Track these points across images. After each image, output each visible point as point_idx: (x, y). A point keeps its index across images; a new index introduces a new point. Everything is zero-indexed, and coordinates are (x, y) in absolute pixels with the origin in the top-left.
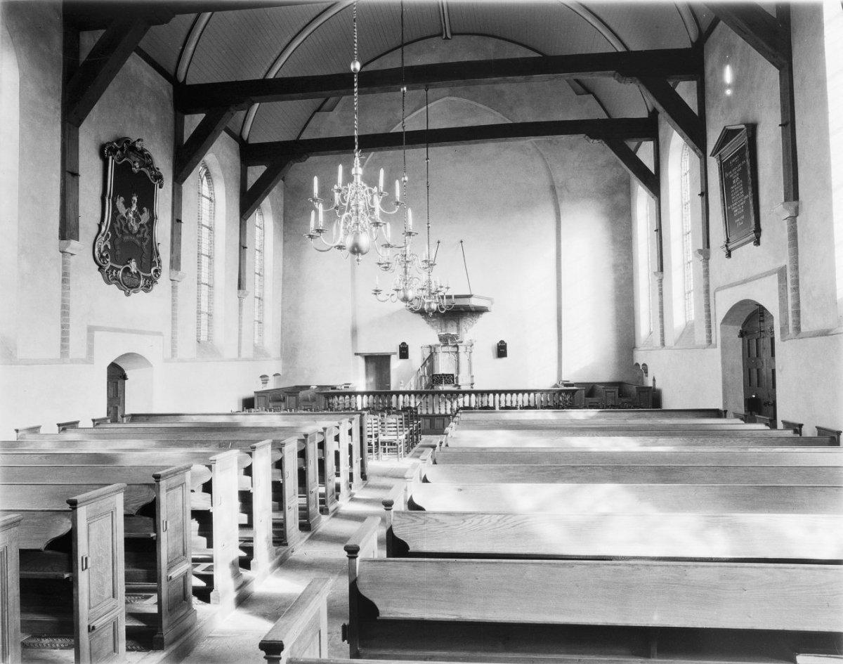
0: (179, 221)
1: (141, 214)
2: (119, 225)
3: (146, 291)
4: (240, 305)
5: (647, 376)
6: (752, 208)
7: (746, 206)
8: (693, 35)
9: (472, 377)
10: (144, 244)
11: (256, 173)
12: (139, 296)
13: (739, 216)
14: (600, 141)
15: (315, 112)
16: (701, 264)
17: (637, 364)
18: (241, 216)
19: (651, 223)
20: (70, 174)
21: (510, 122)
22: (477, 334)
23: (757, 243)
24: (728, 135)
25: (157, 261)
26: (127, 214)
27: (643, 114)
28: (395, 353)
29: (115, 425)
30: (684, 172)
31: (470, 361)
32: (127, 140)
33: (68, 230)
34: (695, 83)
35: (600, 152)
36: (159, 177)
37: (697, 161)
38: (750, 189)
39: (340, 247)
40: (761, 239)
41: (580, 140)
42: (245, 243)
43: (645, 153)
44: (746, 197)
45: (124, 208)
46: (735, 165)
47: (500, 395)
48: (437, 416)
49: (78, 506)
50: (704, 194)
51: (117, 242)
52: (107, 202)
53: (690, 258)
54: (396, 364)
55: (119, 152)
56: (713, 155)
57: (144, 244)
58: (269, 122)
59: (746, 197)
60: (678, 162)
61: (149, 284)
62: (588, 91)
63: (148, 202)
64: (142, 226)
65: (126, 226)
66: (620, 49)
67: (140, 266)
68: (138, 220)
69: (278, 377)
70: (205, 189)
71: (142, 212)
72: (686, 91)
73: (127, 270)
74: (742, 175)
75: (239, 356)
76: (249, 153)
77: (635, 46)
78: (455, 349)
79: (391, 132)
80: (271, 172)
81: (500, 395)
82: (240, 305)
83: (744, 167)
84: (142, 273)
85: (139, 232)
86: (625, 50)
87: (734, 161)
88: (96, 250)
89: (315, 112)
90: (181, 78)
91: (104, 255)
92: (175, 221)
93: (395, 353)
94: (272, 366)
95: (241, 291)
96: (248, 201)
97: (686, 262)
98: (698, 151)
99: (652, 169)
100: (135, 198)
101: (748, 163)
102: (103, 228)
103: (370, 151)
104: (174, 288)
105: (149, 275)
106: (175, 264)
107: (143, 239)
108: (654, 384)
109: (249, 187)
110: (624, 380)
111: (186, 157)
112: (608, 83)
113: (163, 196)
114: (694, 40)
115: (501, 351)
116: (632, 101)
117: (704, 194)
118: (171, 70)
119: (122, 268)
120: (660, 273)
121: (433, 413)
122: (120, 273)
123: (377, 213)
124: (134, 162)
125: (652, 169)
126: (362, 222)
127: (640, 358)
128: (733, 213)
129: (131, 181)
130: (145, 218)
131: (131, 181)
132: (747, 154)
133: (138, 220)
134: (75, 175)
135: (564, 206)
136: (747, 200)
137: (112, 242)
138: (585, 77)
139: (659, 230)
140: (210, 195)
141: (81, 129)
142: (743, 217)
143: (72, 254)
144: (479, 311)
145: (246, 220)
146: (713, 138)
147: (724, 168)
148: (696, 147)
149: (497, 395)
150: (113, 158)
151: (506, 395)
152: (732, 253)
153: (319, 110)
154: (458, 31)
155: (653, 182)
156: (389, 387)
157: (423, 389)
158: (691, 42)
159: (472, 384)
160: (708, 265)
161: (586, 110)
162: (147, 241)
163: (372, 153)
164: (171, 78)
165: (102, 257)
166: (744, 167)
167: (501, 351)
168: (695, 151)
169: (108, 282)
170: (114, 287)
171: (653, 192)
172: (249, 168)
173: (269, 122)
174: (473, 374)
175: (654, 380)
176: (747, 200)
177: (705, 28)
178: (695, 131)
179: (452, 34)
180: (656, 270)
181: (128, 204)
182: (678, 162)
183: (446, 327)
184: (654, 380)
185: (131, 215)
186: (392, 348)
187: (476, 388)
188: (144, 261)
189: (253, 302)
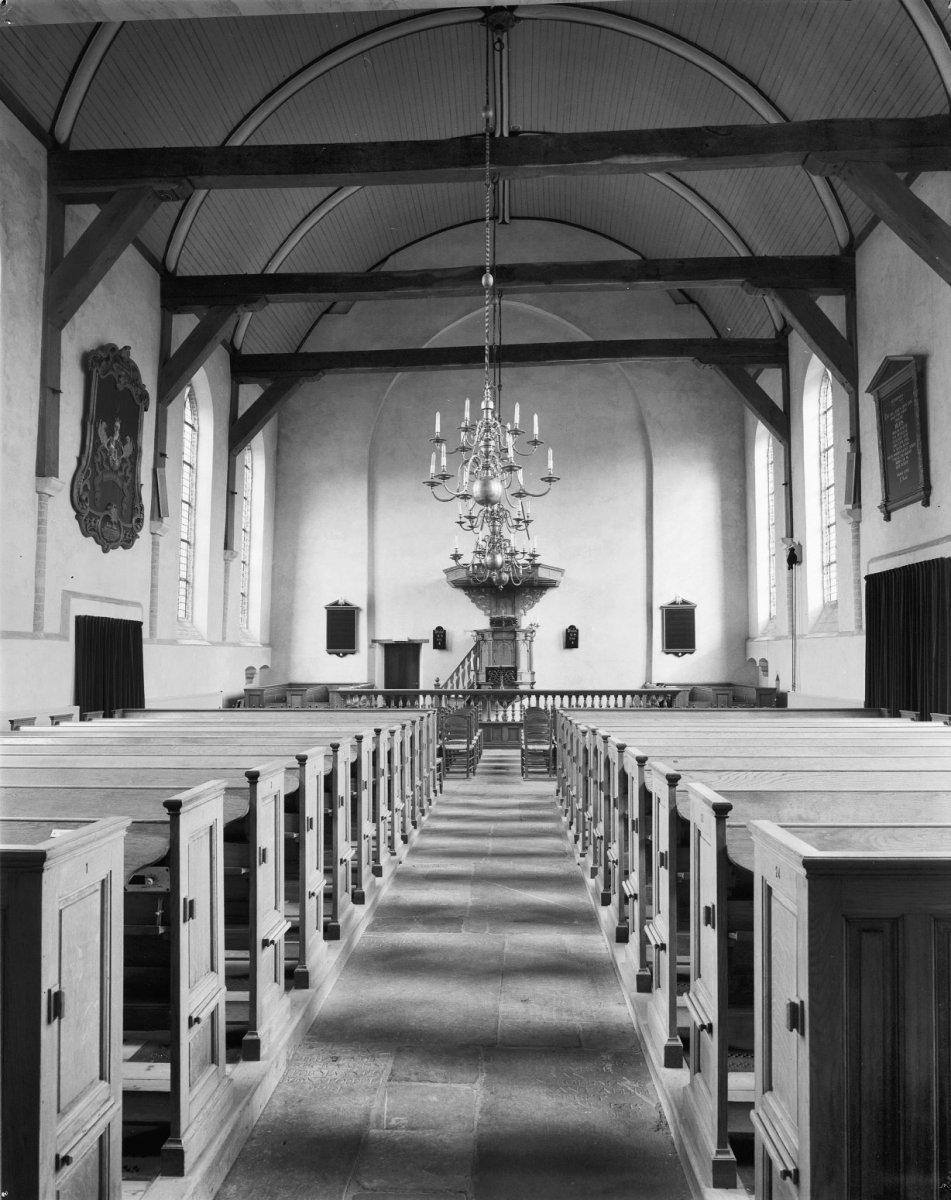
0: (164, 455)
1: (124, 445)
2: (99, 460)
3: (125, 547)
4: (227, 571)
5: (767, 675)
6: (920, 459)
7: (913, 457)
8: (842, 238)
9: (533, 673)
10: (126, 484)
11: (250, 394)
12: (118, 553)
13: (903, 468)
14: (713, 366)
15: (322, 315)
16: (850, 528)
17: (753, 661)
18: (230, 451)
19: (776, 473)
20: (50, 390)
21: (588, 339)
22: (542, 618)
23: (927, 503)
24: (890, 367)
25: (139, 508)
26: (109, 444)
27: (767, 333)
28: (427, 641)
29: (124, 720)
30: (823, 410)
31: (530, 652)
32: (113, 348)
33: (46, 466)
34: (842, 299)
35: (713, 378)
36: (145, 397)
37: (331, 379)
38: (918, 436)
39: (465, 497)
40: (931, 498)
41: (686, 362)
42: (234, 487)
43: (770, 382)
44: (912, 445)
45: (105, 437)
46: (898, 404)
47: (585, 697)
48: (510, 724)
49: (182, 810)
50: (855, 440)
51: (97, 481)
52: (89, 428)
53: (832, 520)
54: (428, 655)
55: (104, 363)
56: (869, 391)
57: (126, 484)
58: (263, 328)
59: (912, 445)
60: (818, 402)
61: (127, 543)
62: (689, 298)
63: (132, 430)
64: (124, 460)
65: (108, 461)
66: (743, 253)
67: (120, 515)
68: (121, 452)
69: (267, 670)
70: (188, 416)
71: (124, 442)
72: (831, 306)
73: (107, 518)
74: (908, 418)
75: (224, 639)
76: (242, 367)
77: (763, 250)
78: (511, 636)
79: (424, 347)
80: (273, 392)
81: (585, 697)
82: (227, 571)
83: (911, 409)
84: (122, 524)
85: (120, 468)
86: (749, 255)
87: (896, 399)
88: (75, 491)
89: (322, 315)
90: (171, 265)
91: (84, 498)
92: (158, 455)
93: (427, 641)
94: (260, 659)
95: (229, 552)
96: (238, 433)
97: (824, 525)
98: (848, 385)
99: (779, 403)
100: (118, 424)
101: (917, 404)
102: (84, 463)
103: (397, 372)
104: (155, 544)
105: (130, 526)
106: (158, 512)
107: (125, 479)
108: (778, 684)
109: (241, 413)
110: (734, 681)
111: (174, 372)
112: (721, 293)
113: (149, 419)
114: (843, 246)
115: (571, 639)
116: (755, 313)
117: (855, 440)
118: (159, 256)
119: (102, 515)
120: (789, 540)
121: (489, 720)
122: (99, 521)
123: (511, 454)
124: (120, 376)
125: (779, 403)
126: (492, 465)
127: (757, 653)
128: (894, 464)
129: (117, 401)
130: (128, 449)
131: (117, 401)
132: (915, 393)
133: (121, 452)
134: (57, 392)
135: (656, 449)
136: (914, 449)
137: (92, 480)
138: (695, 286)
139: (788, 484)
140: (197, 428)
141: (64, 330)
142: (907, 470)
143: (50, 496)
144: (544, 586)
145: (235, 456)
146: (867, 373)
147: (883, 407)
148: (845, 380)
149: (597, 697)
150: (97, 371)
151: (600, 697)
152: (893, 514)
153: (327, 311)
154: (519, 214)
155: (783, 423)
156: (418, 687)
157: (466, 689)
158: (840, 247)
159: (533, 683)
160: (858, 530)
161: (694, 327)
162: (129, 481)
163: (399, 374)
164: (46, 137)
165: (80, 500)
166: (911, 409)
167: (571, 639)
168: (843, 384)
169: (85, 534)
170: (91, 539)
171: (781, 434)
172: (241, 386)
173: (263, 328)
174: (533, 670)
175: (778, 679)
176: (914, 449)
177: (857, 231)
178: (843, 359)
179: (511, 218)
180: (784, 535)
181: (110, 433)
182: (818, 402)
183: (497, 606)
184: (778, 679)
185: (113, 446)
186: (423, 633)
187: (537, 687)
188: (125, 506)
189: (284, 567)
